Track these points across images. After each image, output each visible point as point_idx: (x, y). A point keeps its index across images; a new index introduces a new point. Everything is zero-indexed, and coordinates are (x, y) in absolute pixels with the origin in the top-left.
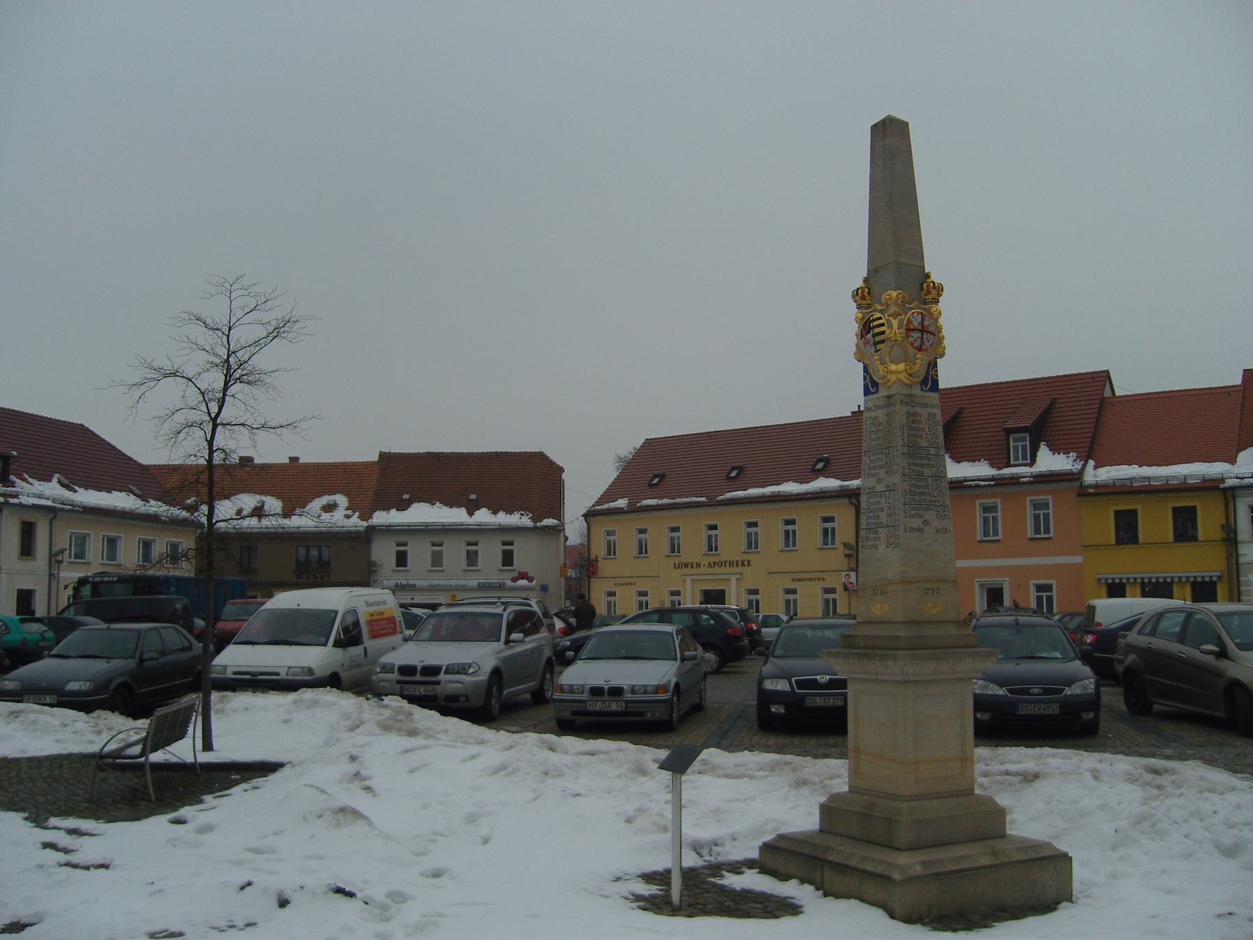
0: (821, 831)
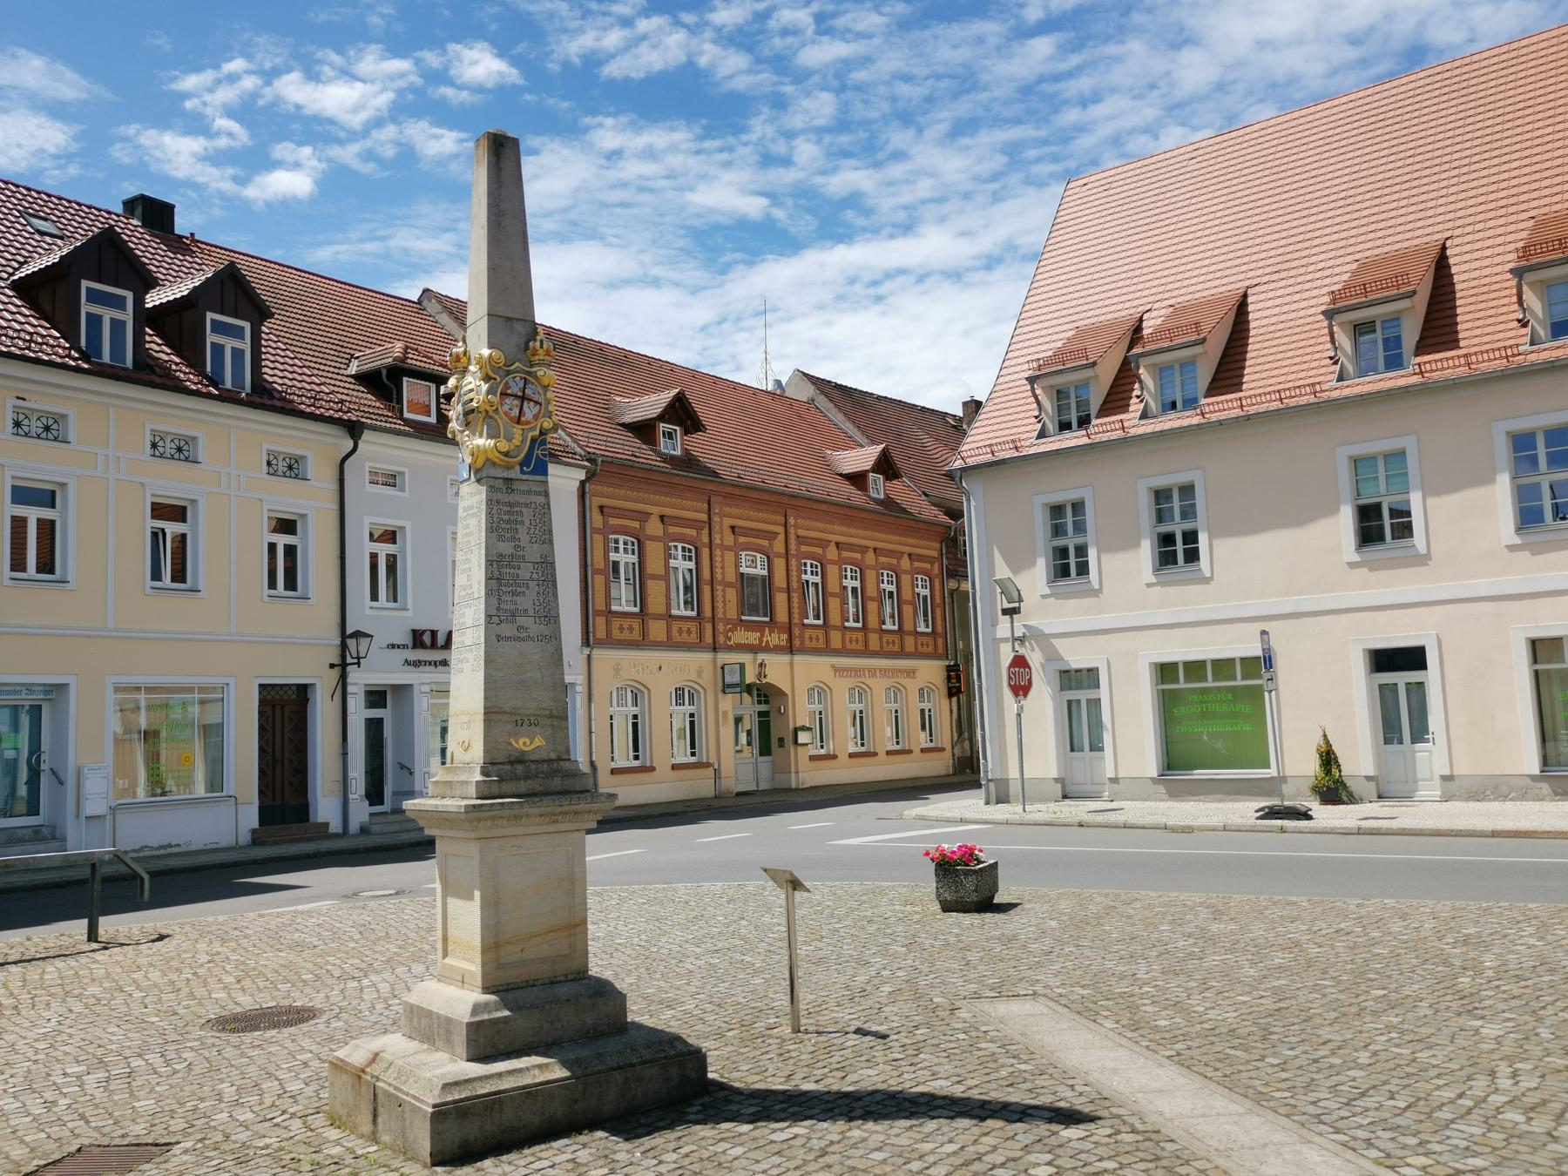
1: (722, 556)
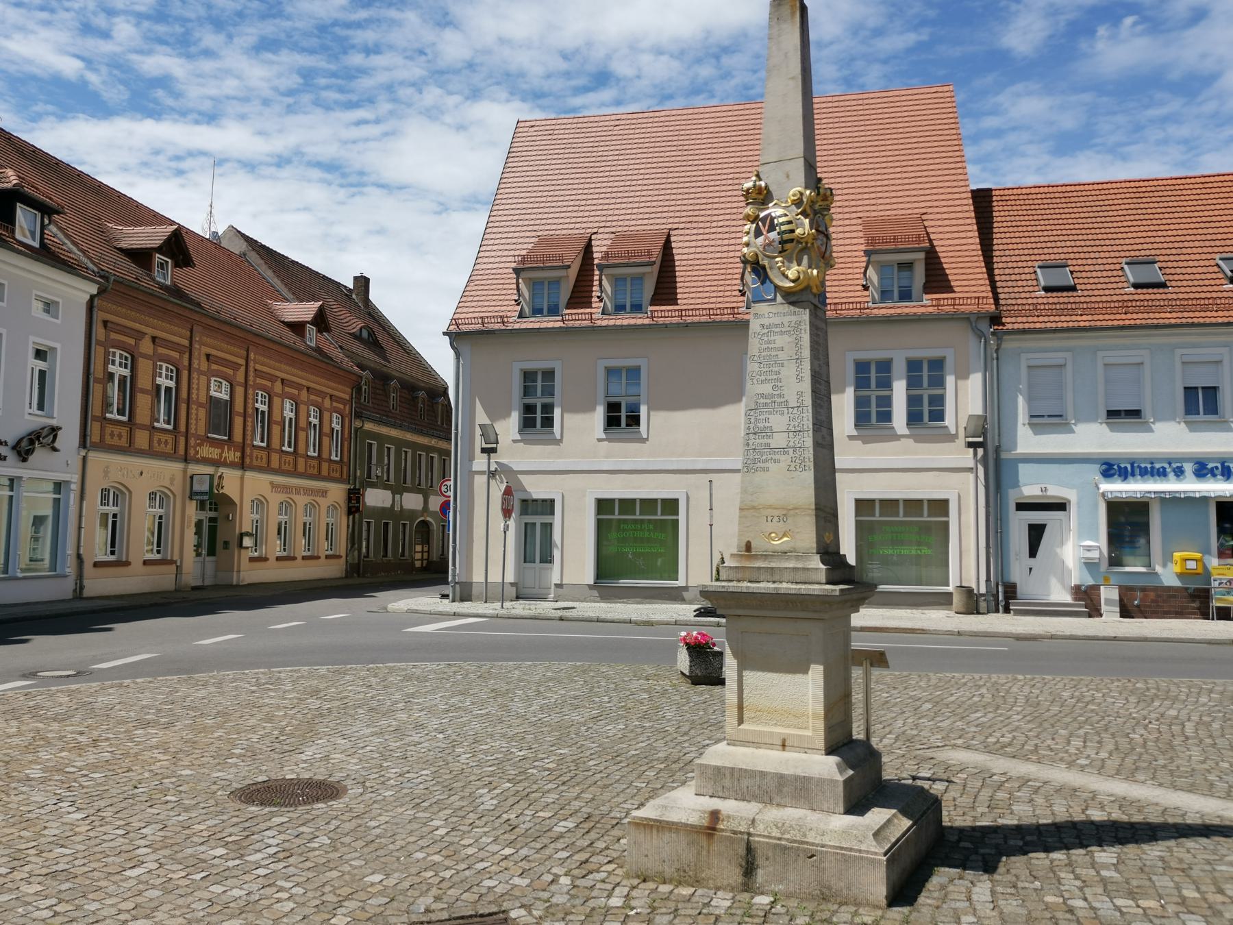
1: (198, 379)
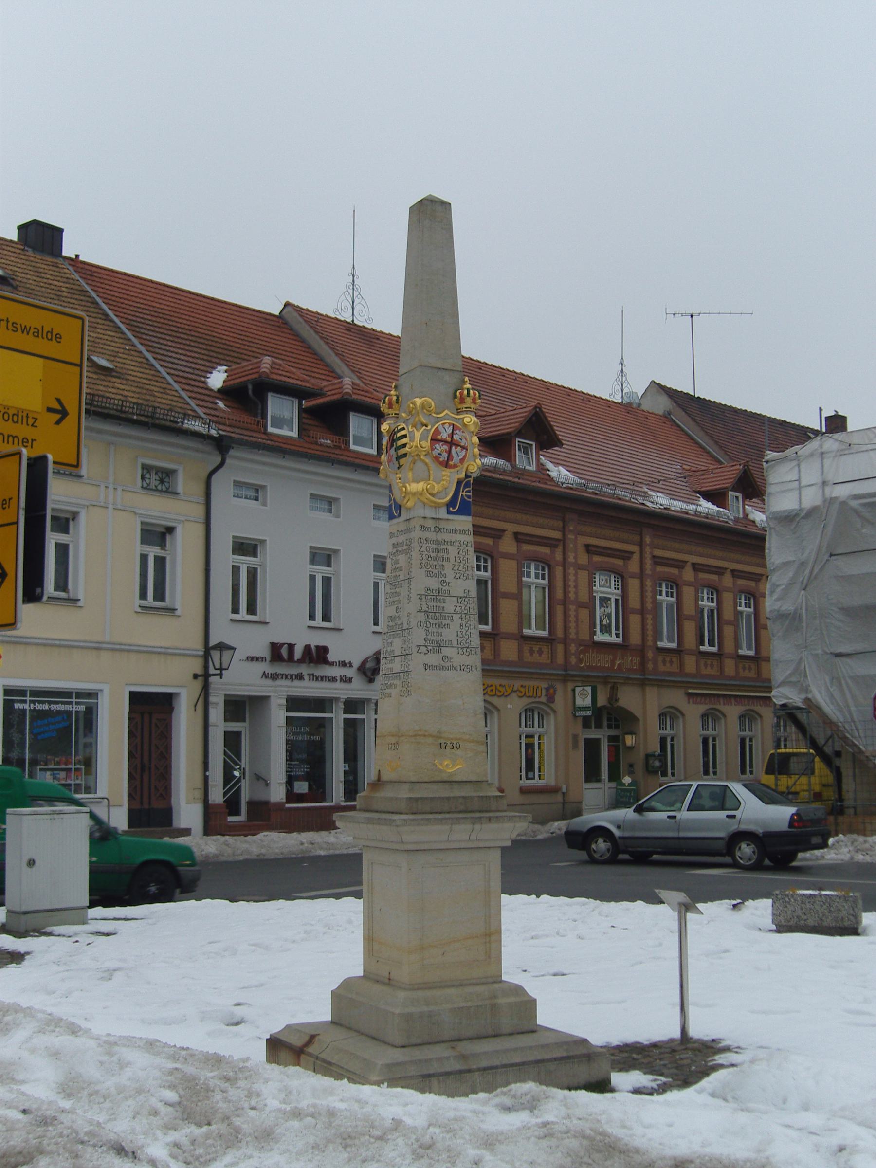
0: (334, 1023)
1: (576, 575)
